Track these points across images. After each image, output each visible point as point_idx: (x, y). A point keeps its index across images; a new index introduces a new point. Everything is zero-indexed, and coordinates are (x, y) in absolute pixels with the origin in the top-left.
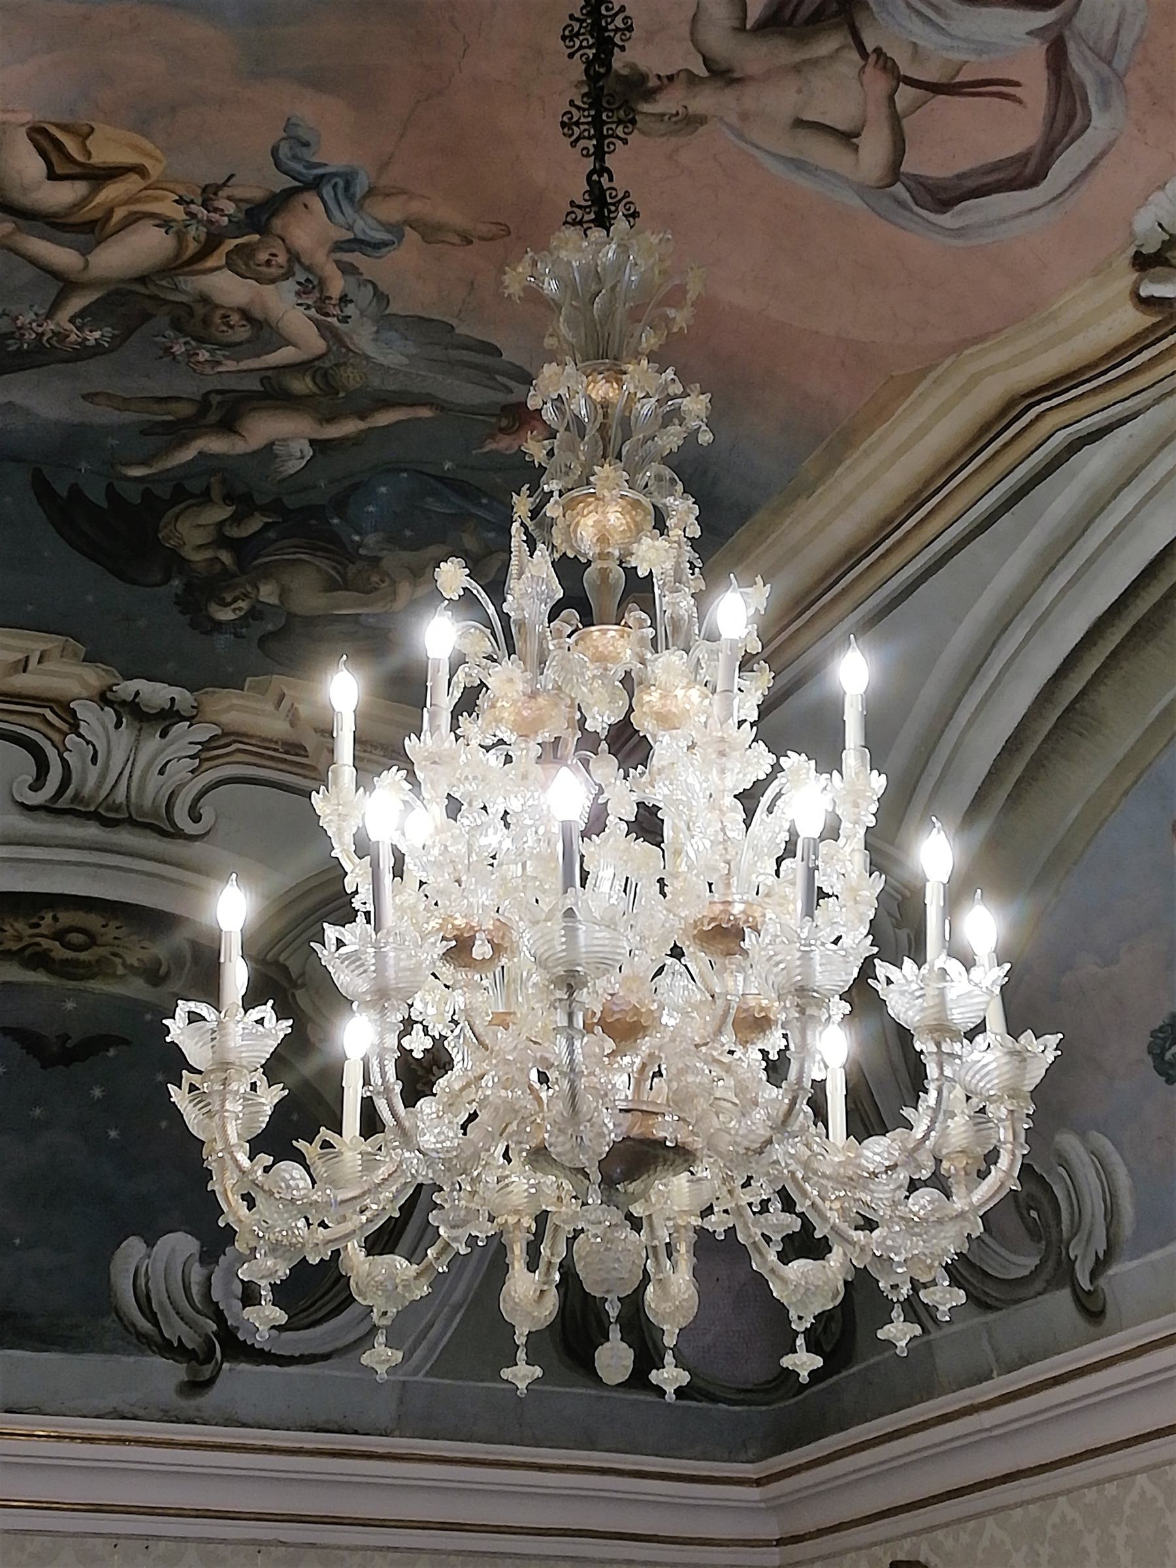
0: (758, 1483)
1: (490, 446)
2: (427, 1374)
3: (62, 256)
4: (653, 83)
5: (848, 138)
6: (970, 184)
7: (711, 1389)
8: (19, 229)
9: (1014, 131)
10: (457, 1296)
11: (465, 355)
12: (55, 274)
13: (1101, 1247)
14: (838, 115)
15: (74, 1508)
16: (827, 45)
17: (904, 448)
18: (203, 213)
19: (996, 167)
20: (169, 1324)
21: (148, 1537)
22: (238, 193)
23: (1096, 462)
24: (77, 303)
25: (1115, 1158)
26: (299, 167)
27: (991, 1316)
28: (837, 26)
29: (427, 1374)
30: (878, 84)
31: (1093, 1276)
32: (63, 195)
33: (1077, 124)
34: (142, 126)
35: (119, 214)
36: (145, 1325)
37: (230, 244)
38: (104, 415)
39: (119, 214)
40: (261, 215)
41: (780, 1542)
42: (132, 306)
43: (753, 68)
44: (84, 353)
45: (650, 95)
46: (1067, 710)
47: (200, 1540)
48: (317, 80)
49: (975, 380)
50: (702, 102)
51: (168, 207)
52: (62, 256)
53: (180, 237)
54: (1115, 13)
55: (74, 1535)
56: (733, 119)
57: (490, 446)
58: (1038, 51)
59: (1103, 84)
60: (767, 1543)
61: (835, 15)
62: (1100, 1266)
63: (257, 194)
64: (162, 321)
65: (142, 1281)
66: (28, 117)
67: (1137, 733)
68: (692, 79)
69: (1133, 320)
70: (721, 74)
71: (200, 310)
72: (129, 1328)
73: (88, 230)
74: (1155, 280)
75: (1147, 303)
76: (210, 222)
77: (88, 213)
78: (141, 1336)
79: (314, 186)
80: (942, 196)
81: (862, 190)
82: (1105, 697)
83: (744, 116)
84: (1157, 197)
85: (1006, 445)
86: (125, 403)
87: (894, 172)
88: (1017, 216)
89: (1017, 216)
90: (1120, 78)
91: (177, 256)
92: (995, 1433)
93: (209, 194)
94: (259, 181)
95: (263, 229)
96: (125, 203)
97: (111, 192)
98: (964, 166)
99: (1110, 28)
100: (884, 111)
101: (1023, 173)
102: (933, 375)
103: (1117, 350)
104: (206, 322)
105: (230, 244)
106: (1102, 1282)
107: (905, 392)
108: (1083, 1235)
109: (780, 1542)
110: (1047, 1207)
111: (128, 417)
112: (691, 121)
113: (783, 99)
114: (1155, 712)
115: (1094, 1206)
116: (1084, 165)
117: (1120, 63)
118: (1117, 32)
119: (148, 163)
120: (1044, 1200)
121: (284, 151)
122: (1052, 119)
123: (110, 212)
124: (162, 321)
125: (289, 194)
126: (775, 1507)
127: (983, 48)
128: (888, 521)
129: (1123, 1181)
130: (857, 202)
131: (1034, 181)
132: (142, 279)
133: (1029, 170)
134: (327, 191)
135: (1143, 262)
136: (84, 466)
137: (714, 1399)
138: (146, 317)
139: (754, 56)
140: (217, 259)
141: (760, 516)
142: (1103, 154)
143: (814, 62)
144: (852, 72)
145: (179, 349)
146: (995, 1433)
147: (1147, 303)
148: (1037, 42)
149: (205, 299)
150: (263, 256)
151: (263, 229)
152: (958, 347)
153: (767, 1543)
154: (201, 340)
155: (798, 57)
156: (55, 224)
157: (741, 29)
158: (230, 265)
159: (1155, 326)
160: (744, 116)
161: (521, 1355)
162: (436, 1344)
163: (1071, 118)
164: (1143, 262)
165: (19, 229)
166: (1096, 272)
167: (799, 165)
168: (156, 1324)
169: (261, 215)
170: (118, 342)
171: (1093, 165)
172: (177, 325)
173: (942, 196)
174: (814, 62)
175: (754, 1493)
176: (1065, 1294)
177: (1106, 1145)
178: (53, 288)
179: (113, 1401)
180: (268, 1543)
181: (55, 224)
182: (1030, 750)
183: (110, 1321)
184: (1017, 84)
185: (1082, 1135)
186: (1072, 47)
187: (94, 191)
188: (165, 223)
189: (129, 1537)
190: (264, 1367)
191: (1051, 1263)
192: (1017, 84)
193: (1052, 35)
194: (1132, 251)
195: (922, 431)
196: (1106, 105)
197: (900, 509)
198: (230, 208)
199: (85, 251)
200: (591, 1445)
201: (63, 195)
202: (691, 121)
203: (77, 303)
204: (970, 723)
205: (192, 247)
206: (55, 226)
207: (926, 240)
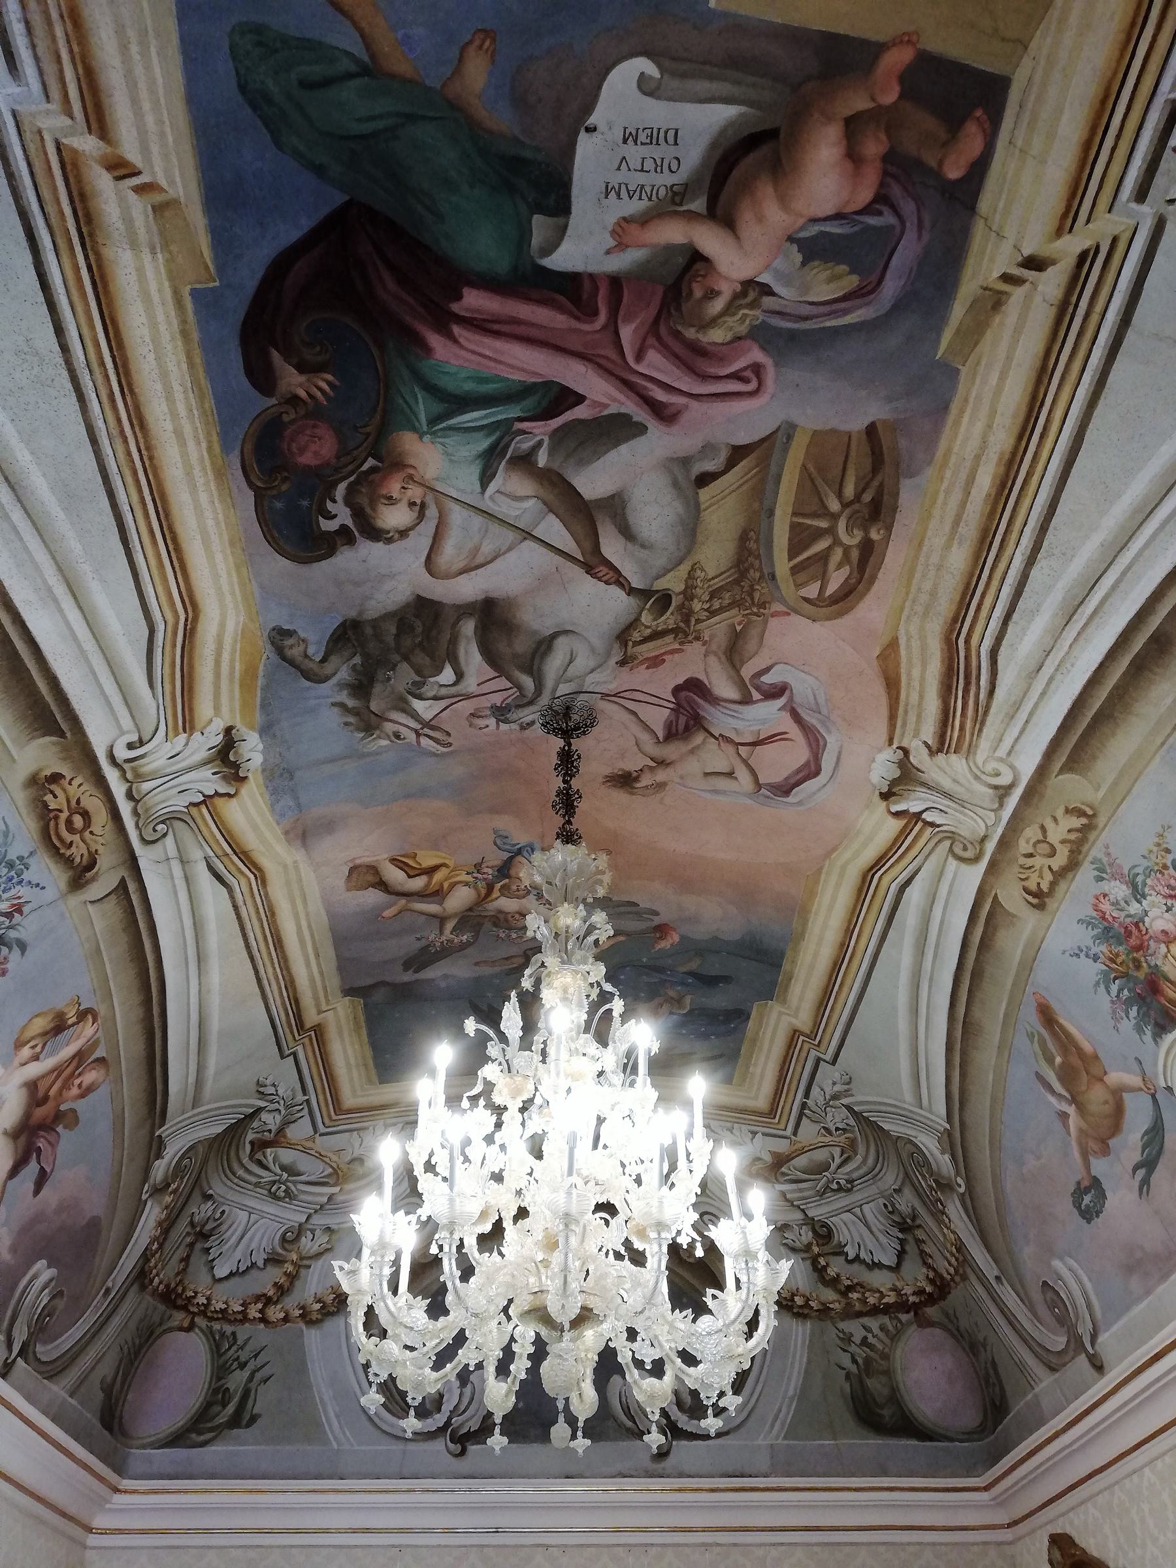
0: (986, 1489)
1: (658, 947)
2: (785, 1438)
3: (433, 908)
4: (635, 774)
5: (730, 775)
6: (792, 781)
7: (949, 1434)
8: (408, 901)
9: (796, 754)
10: (791, 1392)
11: (623, 909)
12: (434, 916)
13: (1091, 1326)
14: (722, 767)
15: (763, 1529)
16: (699, 738)
17: (831, 907)
18: (480, 876)
19: (798, 771)
20: (641, 1422)
21: (646, 1545)
22: (490, 864)
23: (915, 895)
24: (450, 926)
25: (1080, 1272)
26: (508, 847)
27: (1057, 1375)
28: (698, 730)
29: (785, 1438)
30: (730, 749)
31: (1093, 1344)
32: (419, 883)
33: (821, 743)
34: (435, 846)
35: (446, 885)
36: (629, 1424)
37: (498, 886)
38: (486, 970)
39: (446, 885)
40: (505, 870)
41: (1009, 1526)
42: (470, 919)
43: (673, 757)
44: (463, 947)
45: (636, 779)
46: (964, 1022)
47: (675, 1545)
48: (495, 810)
49: (843, 868)
50: (661, 776)
51: (464, 877)
52: (433, 908)
53: (476, 888)
54: (809, 690)
55: (608, 1546)
56: (678, 780)
57: (658, 947)
58: (786, 716)
59: (823, 723)
60: (1001, 1527)
61: (694, 726)
62: (1094, 1337)
63: (498, 862)
64: (488, 925)
65: (624, 1399)
66: (386, 856)
67: (999, 1030)
68: (651, 768)
69: (896, 825)
70: (662, 763)
71: (501, 916)
72: (621, 1425)
73: (438, 894)
74: (895, 803)
75: (897, 814)
76: (485, 879)
77: (434, 886)
78: (628, 1430)
79: (519, 852)
80: (785, 789)
81: (748, 795)
82: (977, 1013)
83: (682, 777)
84: (874, 765)
85: (873, 897)
86: (493, 963)
87: (758, 786)
88: (819, 790)
89: (819, 790)
90: (828, 718)
91: (479, 896)
92: (1074, 1447)
93: (478, 867)
94: (496, 858)
95: (508, 876)
96: (446, 880)
97: (438, 876)
98: (785, 774)
99: (811, 698)
100: (738, 759)
101: (811, 770)
102: (824, 871)
103: (896, 840)
104: (507, 921)
105: (498, 886)
106: (1097, 1347)
107: (817, 882)
108: (1081, 1319)
109: (1009, 1526)
110: (1061, 1306)
111: (497, 969)
112: (661, 786)
113: (693, 766)
114: (1001, 1016)
115: (1081, 1302)
116: (835, 759)
117: (825, 711)
118: (815, 699)
119: (447, 862)
120: (1059, 1303)
121: (498, 842)
122: (810, 745)
123: (442, 885)
124: (488, 925)
125: (511, 858)
126: (1000, 1503)
127: (764, 722)
128: (842, 945)
129: (1089, 1286)
130: (749, 802)
131: (817, 772)
132: (470, 909)
133: (813, 768)
134: (525, 854)
135: (886, 796)
136: (489, 995)
137: (951, 1440)
138: (480, 925)
139: (671, 751)
140: (496, 893)
141: (789, 953)
142: (840, 753)
143: (698, 747)
144: (716, 747)
145: (502, 935)
146: (1074, 1447)
147: (897, 814)
148: (784, 713)
149: (500, 912)
150: (515, 888)
151: (508, 876)
152: (828, 855)
153: (1001, 1527)
154: (510, 929)
155: (690, 747)
156: (421, 895)
157: (659, 742)
158: (503, 895)
159: (905, 826)
160: (682, 777)
161: (497, 1430)
162: (785, 1421)
163: (818, 741)
164: (886, 796)
165: (408, 901)
166: (867, 806)
167: (716, 792)
168: (635, 1422)
169: (505, 870)
170: (476, 937)
171: (838, 759)
172: (495, 925)
173: (785, 789)
174: (698, 747)
175: (984, 1496)
176: (1084, 1355)
177: (1072, 1262)
178: (437, 923)
179: (619, 1467)
180: (710, 1545)
181: (421, 895)
182: (958, 1046)
183: (610, 1423)
184: (785, 733)
185: (1061, 1259)
186: (800, 711)
187: (431, 879)
188: (467, 884)
189: (636, 1545)
190: (694, 1442)
191: (1072, 1340)
192: (785, 733)
193: (788, 708)
194: (877, 793)
195: (834, 898)
196: (829, 732)
197: (845, 937)
198: (490, 871)
199: (441, 904)
200: (885, 1473)
201: (419, 883)
202: (661, 786)
203: (450, 926)
204: (926, 1038)
205: (483, 892)
206: (423, 896)
207: (786, 810)
